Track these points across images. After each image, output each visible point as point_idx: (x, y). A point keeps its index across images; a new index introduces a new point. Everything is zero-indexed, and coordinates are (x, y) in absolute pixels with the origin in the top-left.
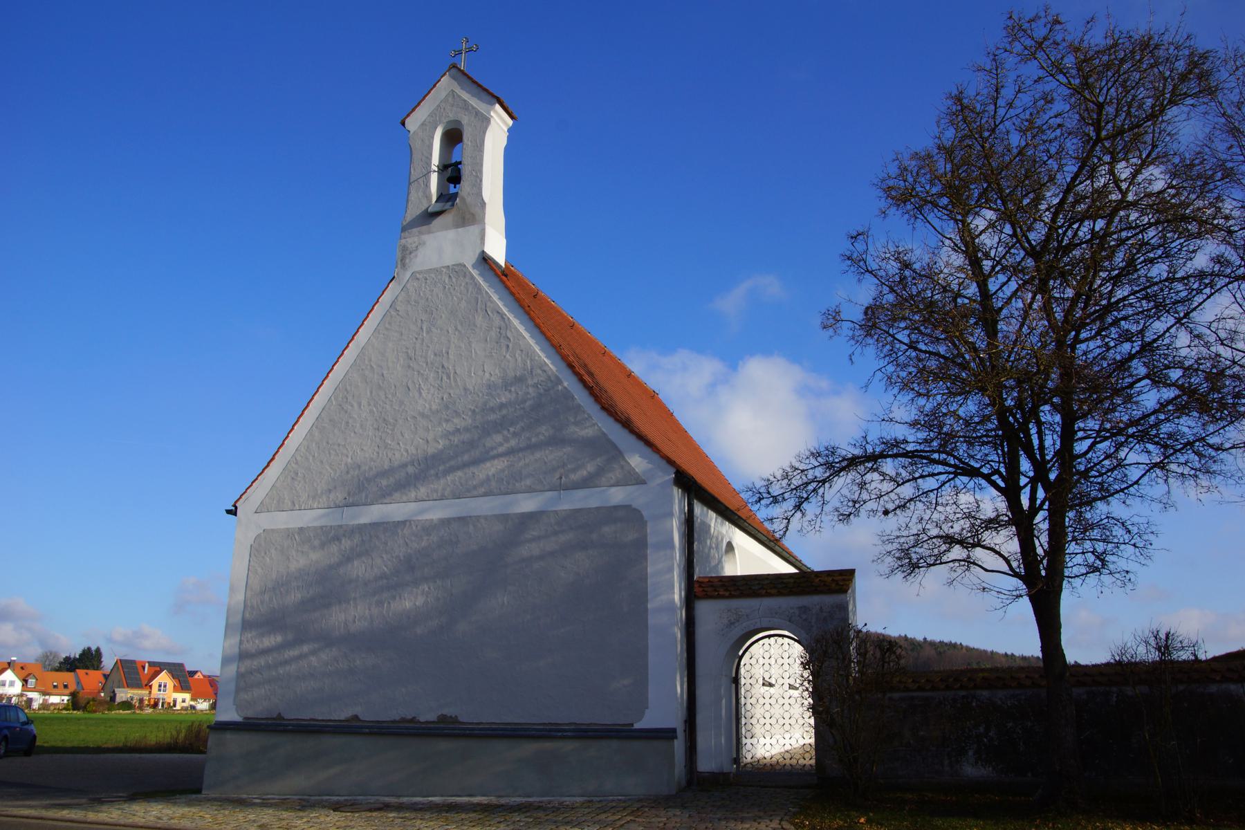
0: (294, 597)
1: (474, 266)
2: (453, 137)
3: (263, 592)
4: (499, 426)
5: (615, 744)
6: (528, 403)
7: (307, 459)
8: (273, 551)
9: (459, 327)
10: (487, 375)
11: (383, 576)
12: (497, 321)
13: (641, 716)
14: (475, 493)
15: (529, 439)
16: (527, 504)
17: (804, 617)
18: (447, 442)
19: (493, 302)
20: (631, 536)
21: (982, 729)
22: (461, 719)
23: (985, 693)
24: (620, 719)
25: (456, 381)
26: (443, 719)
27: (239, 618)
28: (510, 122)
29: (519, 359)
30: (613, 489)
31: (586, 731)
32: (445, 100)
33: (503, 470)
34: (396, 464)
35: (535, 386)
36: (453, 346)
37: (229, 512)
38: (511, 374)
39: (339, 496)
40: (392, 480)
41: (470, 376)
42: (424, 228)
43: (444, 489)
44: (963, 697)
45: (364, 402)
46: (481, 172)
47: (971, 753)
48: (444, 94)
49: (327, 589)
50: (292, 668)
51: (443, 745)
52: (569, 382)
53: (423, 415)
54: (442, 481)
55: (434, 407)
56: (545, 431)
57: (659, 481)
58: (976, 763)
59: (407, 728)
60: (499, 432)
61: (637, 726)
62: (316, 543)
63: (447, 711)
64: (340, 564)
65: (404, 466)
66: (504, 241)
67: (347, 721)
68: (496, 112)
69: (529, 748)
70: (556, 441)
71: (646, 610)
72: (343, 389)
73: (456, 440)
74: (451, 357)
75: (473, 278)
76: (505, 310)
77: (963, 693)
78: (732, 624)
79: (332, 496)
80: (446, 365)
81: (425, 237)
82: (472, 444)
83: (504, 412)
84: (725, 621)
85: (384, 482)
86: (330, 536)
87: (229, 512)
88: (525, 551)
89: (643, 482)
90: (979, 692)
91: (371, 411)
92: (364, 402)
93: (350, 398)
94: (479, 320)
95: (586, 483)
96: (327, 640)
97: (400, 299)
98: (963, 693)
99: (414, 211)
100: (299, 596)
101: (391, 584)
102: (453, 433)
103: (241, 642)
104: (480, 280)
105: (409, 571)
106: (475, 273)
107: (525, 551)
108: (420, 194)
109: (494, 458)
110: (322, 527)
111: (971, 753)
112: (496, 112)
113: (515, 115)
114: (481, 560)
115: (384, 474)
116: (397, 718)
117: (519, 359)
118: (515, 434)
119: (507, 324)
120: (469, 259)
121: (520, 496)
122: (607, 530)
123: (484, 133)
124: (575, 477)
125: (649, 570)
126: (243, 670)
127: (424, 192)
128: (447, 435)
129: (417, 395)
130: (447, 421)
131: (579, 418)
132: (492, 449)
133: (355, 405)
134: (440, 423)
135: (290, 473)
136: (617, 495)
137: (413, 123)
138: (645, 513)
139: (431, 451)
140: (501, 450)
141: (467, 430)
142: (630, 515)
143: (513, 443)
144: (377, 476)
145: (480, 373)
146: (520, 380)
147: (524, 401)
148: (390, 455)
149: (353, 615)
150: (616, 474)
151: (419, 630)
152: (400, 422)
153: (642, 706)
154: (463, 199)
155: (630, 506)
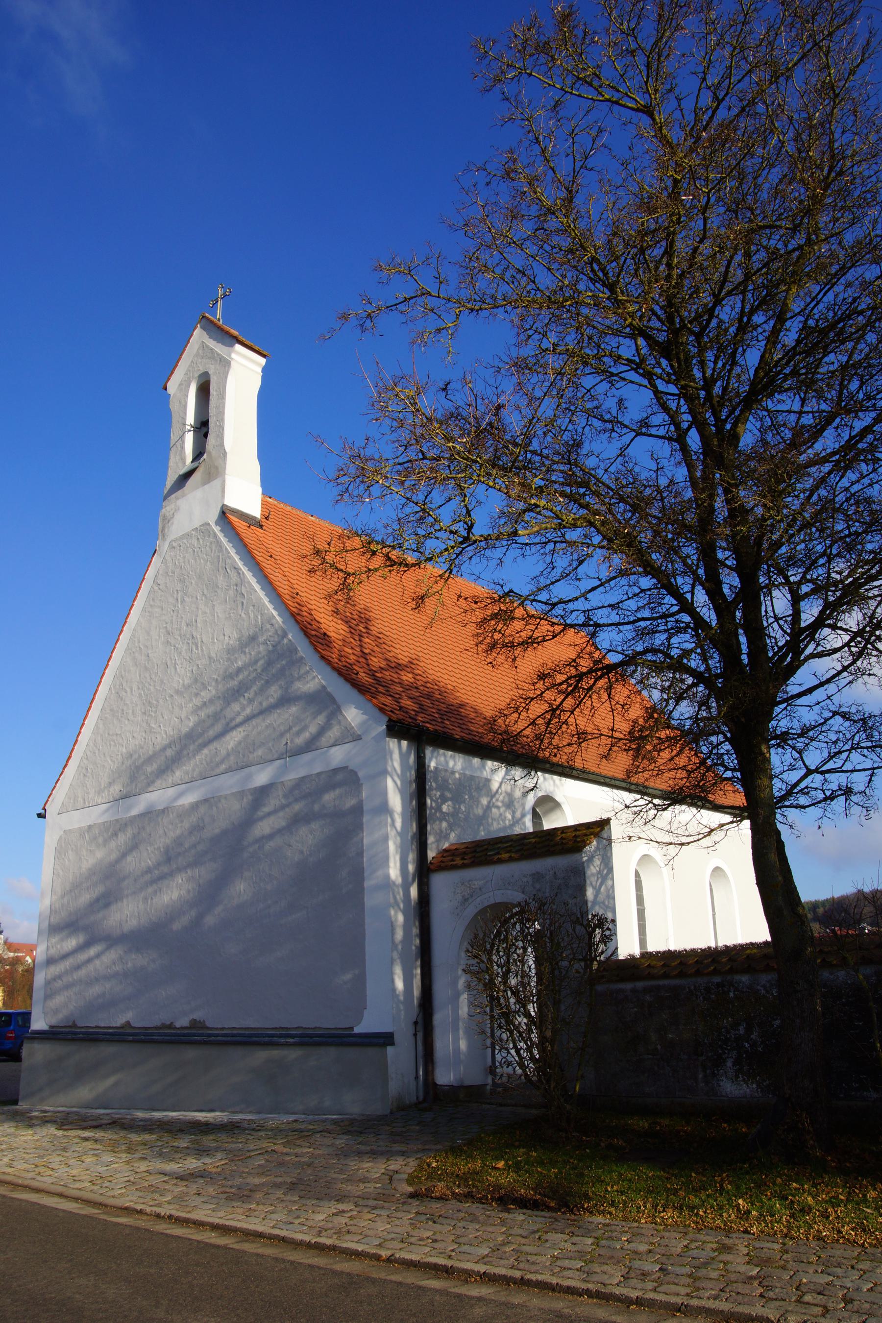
0: (85, 898)
1: (217, 523)
2: (204, 391)
3: (63, 896)
4: (235, 694)
5: (332, 1051)
6: (261, 663)
7: (94, 753)
8: (70, 852)
9: (205, 592)
10: (227, 638)
11: (149, 870)
12: (234, 578)
13: (359, 1018)
14: (218, 771)
15: (261, 703)
16: (262, 777)
17: (538, 886)
18: (196, 718)
19: (230, 557)
20: (351, 802)
21: (742, 1030)
22: (208, 1024)
23: (745, 978)
24: (329, 1021)
25: (202, 650)
26: (194, 1024)
27: (46, 924)
28: (263, 361)
29: (252, 616)
30: (334, 750)
31: (310, 1036)
32: (197, 355)
33: (240, 743)
34: (158, 748)
35: (265, 643)
36: (200, 612)
37: (40, 816)
38: (246, 633)
39: (116, 789)
40: (155, 766)
41: (213, 643)
42: (180, 492)
43: (194, 770)
44: (718, 985)
45: (135, 687)
46: (223, 420)
47: (729, 1063)
48: (196, 347)
49: (109, 885)
50: (82, 973)
51: (191, 1053)
52: (294, 636)
53: (177, 692)
54: (192, 762)
55: (187, 682)
56: (274, 692)
57: (374, 733)
58: (737, 1077)
59: (165, 1035)
60: (236, 700)
61: (357, 1030)
62: (100, 840)
63: (197, 1016)
64: (118, 860)
65: (164, 749)
66: (260, 489)
67: (122, 1027)
68: (239, 354)
69: (261, 1055)
70: (285, 701)
71: (363, 889)
72: (119, 676)
73: (202, 714)
74: (199, 625)
75: (215, 535)
76: (240, 564)
77: (717, 979)
78: (466, 900)
79: (111, 790)
80: (195, 634)
81: (179, 502)
82: (216, 717)
83: (241, 677)
84: (459, 897)
85: (149, 769)
86: (115, 828)
87: (40, 816)
88: (264, 827)
89: (358, 738)
90: (737, 977)
91: (140, 695)
92: (135, 687)
93: (124, 684)
94: (221, 580)
95: (310, 746)
96: (111, 940)
97: (161, 572)
98: (717, 979)
99: (172, 478)
100: (88, 897)
101: (157, 877)
102: (200, 708)
103: (48, 949)
104: (221, 536)
105: (171, 861)
106: (217, 529)
107: (264, 827)
108: (178, 457)
109: (237, 726)
110: (104, 823)
111: (729, 1063)
112: (239, 354)
113: (265, 353)
114: (225, 847)
115: (150, 760)
116: (159, 1024)
117: (252, 616)
118: (251, 701)
119: (242, 580)
120: (213, 515)
121: (253, 769)
122: (328, 797)
123: (226, 378)
124: (300, 741)
125: (365, 841)
126: (49, 977)
127: (180, 455)
128: (196, 710)
129: (173, 670)
130: (197, 695)
131: (302, 672)
132: (233, 719)
133: (128, 690)
134: (191, 700)
135: (83, 771)
136: (338, 755)
137: (173, 387)
138: (360, 774)
139: (185, 730)
140: (239, 719)
141: (211, 701)
142: (346, 778)
143: (248, 711)
144: (144, 763)
145: (222, 637)
146: (253, 638)
147: (256, 662)
148: (153, 739)
149: (128, 913)
150: (334, 733)
151: (176, 926)
152: (161, 702)
153: (359, 1006)
154: (210, 453)
155: (347, 767)
